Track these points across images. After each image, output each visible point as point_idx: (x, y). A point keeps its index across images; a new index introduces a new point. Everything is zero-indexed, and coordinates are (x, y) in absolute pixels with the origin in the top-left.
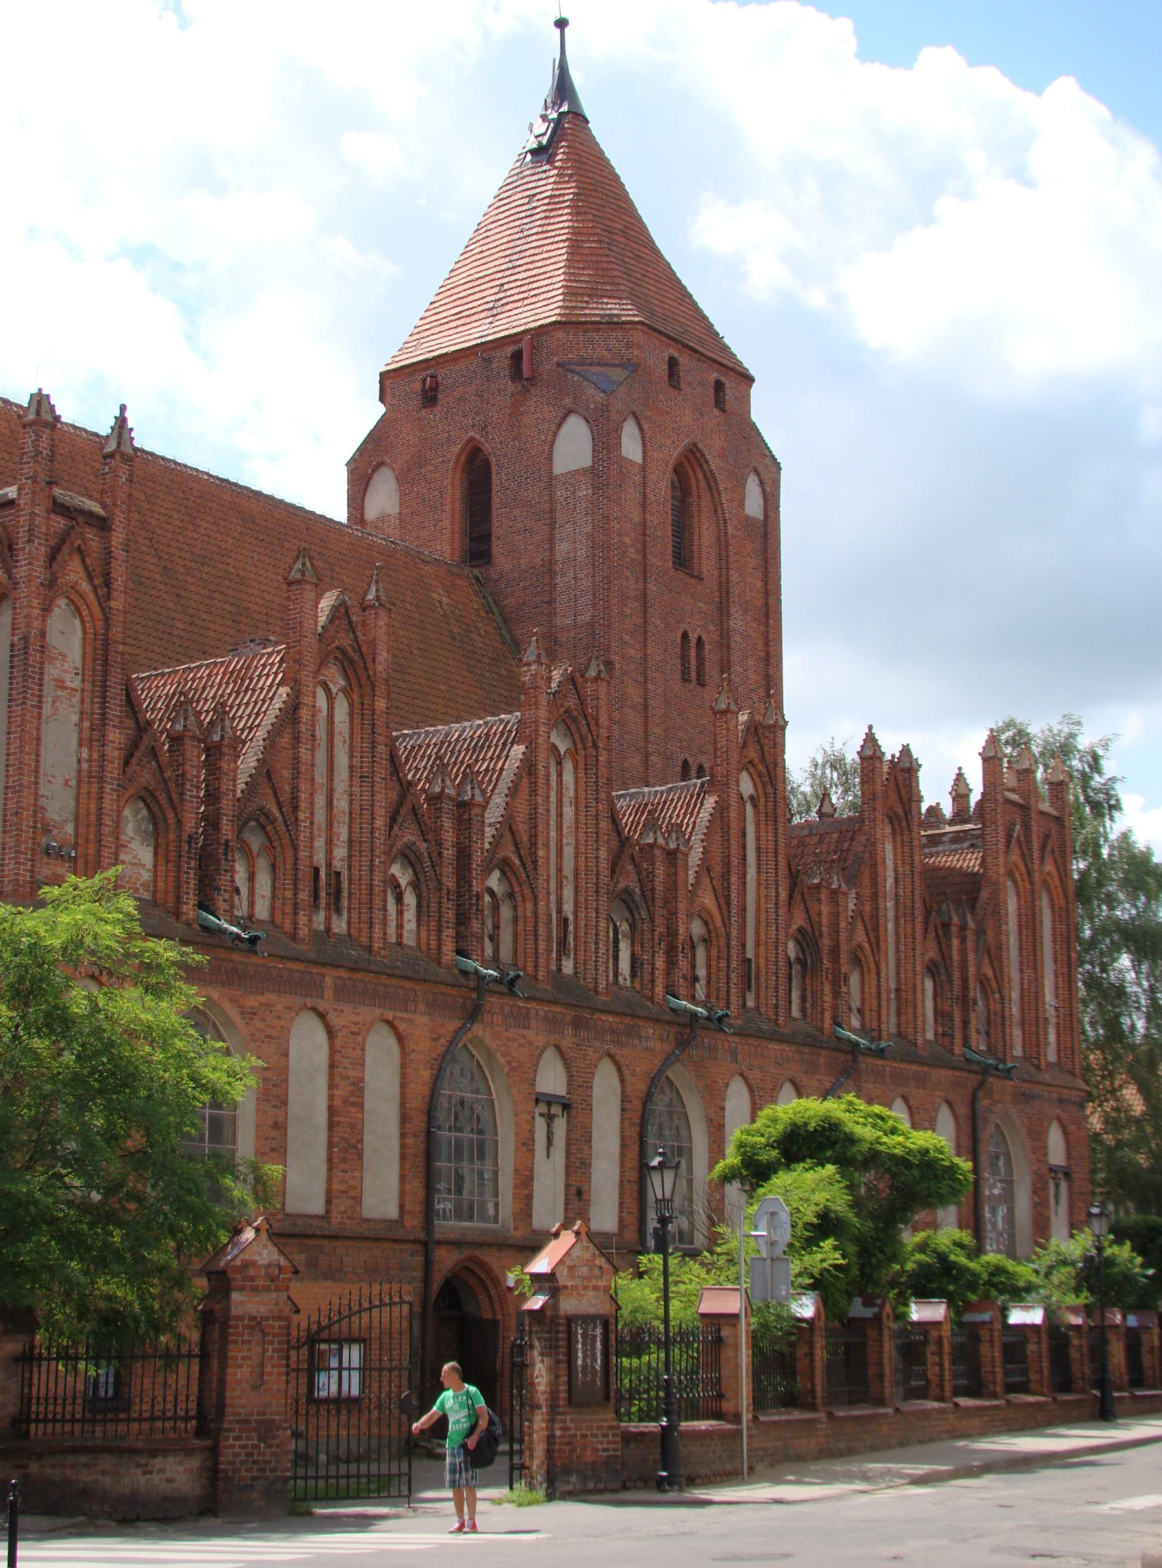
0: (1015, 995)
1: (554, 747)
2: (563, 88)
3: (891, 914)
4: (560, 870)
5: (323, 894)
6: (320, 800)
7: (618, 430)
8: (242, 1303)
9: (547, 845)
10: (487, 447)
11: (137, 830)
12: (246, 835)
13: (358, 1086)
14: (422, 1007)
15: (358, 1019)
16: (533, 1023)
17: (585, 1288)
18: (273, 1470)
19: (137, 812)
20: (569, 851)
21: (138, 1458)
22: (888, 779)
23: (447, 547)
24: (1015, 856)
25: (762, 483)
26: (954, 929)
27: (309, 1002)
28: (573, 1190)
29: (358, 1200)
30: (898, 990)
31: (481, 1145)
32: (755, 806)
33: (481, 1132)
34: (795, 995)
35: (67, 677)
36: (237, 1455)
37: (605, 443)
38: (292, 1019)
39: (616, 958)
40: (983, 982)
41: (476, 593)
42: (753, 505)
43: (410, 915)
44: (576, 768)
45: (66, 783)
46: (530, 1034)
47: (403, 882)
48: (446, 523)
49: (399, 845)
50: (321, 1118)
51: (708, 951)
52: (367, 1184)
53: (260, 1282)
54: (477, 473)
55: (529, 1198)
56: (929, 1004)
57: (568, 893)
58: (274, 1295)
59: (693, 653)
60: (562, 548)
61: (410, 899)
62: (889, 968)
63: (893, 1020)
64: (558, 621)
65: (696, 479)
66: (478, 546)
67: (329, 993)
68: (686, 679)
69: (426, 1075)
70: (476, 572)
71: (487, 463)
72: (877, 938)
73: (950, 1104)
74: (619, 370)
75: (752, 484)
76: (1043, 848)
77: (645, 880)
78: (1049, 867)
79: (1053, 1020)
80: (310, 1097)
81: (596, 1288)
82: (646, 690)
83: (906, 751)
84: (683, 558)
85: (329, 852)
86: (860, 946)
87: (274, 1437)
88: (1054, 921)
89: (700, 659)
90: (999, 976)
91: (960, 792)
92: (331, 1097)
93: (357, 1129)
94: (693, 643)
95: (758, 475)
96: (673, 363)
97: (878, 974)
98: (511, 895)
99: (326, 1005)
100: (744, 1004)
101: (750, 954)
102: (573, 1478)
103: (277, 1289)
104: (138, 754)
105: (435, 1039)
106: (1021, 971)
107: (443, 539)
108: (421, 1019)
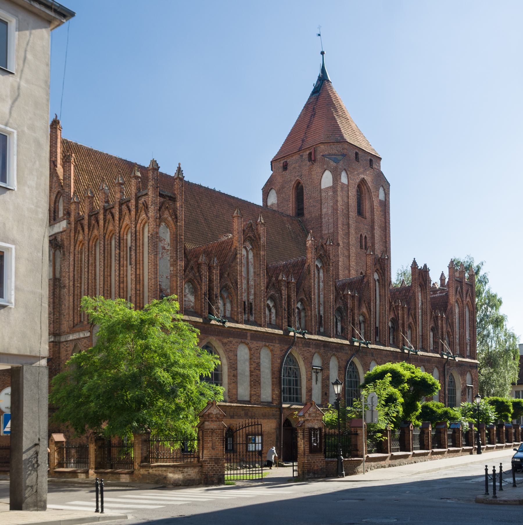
0: (457, 337)
1: (317, 265)
2: (323, 70)
3: (420, 314)
4: (319, 302)
5: (247, 309)
6: (244, 282)
7: (340, 175)
8: (208, 425)
9: (314, 294)
10: (302, 182)
11: (189, 291)
12: (223, 292)
13: (258, 364)
14: (277, 342)
15: (258, 345)
16: (311, 346)
17: (314, 420)
18: (220, 472)
19: (189, 286)
20: (322, 296)
21: (179, 469)
22: (420, 274)
23: (291, 212)
24: (458, 297)
25: (384, 190)
26: (439, 318)
27: (243, 340)
28: (324, 393)
29: (259, 396)
30: (422, 335)
31: (296, 381)
32: (379, 282)
33: (296, 377)
34: (391, 337)
35: (166, 246)
36: (208, 468)
37: (336, 178)
38: (238, 346)
39: (337, 327)
40: (448, 333)
41: (299, 225)
42: (382, 196)
43: (273, 315)
44: (324, 272)
45: (167, 277)
46: (310, 349)
47: (271, 306)
48: (291, 205)
49: (269, 295)
50: (248, 373)
51: (365, 325)
52: (262, 391)
53: (214, 419)
54: (299, 190)
55: (311, 395)
56: (432, 339)
57: (322, 308)
58: (218, 423)
59: (364, 241)
60: (324, 210)
61: (273, 311)
62: (419, 329)
63: (421, 344)
64: (323, 232)
65: (364, 188)
66: (300, 211)
67: (249, 338)
68: (361, 247)
69: (279, 361)
70: (299, 219)
71: (302, 186)
72: (416, 321)
73: (437, 368)
74: (340, 157)
75: (381, 190)
76: (467, 294)
77: (345, 304)
78: (468, 299)
79: (469, 344)
80: (244, 367)
81: (317, 420)
82: (349, 251)
83: (425, 266)
84: (360, 212)
85: (248, 297)
86: (411, 323)
87: (220, 463)
88: (469, 315)
89: (366, 242)
90: (453, 331)
91: (442, 278)
92: (250, 368)
93: (259, 376)
94: (364, 238)
95: (383, 187)
96: (357, 154)
97: (416, 331)
98: (304, 309)
99: (248, 341)
100: (376, 340)
101: (377, 325)
102: (311, 474)
103: (219, 421)
104: (188, 269)
105: (282, 351)
106: (460, 330)
107: (290, 209)
108: (277, 345)
